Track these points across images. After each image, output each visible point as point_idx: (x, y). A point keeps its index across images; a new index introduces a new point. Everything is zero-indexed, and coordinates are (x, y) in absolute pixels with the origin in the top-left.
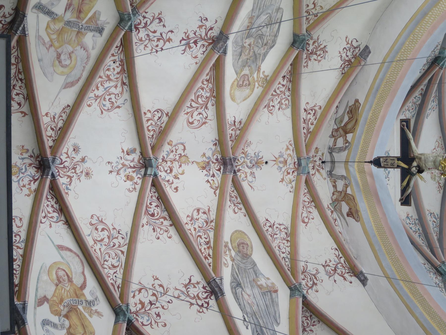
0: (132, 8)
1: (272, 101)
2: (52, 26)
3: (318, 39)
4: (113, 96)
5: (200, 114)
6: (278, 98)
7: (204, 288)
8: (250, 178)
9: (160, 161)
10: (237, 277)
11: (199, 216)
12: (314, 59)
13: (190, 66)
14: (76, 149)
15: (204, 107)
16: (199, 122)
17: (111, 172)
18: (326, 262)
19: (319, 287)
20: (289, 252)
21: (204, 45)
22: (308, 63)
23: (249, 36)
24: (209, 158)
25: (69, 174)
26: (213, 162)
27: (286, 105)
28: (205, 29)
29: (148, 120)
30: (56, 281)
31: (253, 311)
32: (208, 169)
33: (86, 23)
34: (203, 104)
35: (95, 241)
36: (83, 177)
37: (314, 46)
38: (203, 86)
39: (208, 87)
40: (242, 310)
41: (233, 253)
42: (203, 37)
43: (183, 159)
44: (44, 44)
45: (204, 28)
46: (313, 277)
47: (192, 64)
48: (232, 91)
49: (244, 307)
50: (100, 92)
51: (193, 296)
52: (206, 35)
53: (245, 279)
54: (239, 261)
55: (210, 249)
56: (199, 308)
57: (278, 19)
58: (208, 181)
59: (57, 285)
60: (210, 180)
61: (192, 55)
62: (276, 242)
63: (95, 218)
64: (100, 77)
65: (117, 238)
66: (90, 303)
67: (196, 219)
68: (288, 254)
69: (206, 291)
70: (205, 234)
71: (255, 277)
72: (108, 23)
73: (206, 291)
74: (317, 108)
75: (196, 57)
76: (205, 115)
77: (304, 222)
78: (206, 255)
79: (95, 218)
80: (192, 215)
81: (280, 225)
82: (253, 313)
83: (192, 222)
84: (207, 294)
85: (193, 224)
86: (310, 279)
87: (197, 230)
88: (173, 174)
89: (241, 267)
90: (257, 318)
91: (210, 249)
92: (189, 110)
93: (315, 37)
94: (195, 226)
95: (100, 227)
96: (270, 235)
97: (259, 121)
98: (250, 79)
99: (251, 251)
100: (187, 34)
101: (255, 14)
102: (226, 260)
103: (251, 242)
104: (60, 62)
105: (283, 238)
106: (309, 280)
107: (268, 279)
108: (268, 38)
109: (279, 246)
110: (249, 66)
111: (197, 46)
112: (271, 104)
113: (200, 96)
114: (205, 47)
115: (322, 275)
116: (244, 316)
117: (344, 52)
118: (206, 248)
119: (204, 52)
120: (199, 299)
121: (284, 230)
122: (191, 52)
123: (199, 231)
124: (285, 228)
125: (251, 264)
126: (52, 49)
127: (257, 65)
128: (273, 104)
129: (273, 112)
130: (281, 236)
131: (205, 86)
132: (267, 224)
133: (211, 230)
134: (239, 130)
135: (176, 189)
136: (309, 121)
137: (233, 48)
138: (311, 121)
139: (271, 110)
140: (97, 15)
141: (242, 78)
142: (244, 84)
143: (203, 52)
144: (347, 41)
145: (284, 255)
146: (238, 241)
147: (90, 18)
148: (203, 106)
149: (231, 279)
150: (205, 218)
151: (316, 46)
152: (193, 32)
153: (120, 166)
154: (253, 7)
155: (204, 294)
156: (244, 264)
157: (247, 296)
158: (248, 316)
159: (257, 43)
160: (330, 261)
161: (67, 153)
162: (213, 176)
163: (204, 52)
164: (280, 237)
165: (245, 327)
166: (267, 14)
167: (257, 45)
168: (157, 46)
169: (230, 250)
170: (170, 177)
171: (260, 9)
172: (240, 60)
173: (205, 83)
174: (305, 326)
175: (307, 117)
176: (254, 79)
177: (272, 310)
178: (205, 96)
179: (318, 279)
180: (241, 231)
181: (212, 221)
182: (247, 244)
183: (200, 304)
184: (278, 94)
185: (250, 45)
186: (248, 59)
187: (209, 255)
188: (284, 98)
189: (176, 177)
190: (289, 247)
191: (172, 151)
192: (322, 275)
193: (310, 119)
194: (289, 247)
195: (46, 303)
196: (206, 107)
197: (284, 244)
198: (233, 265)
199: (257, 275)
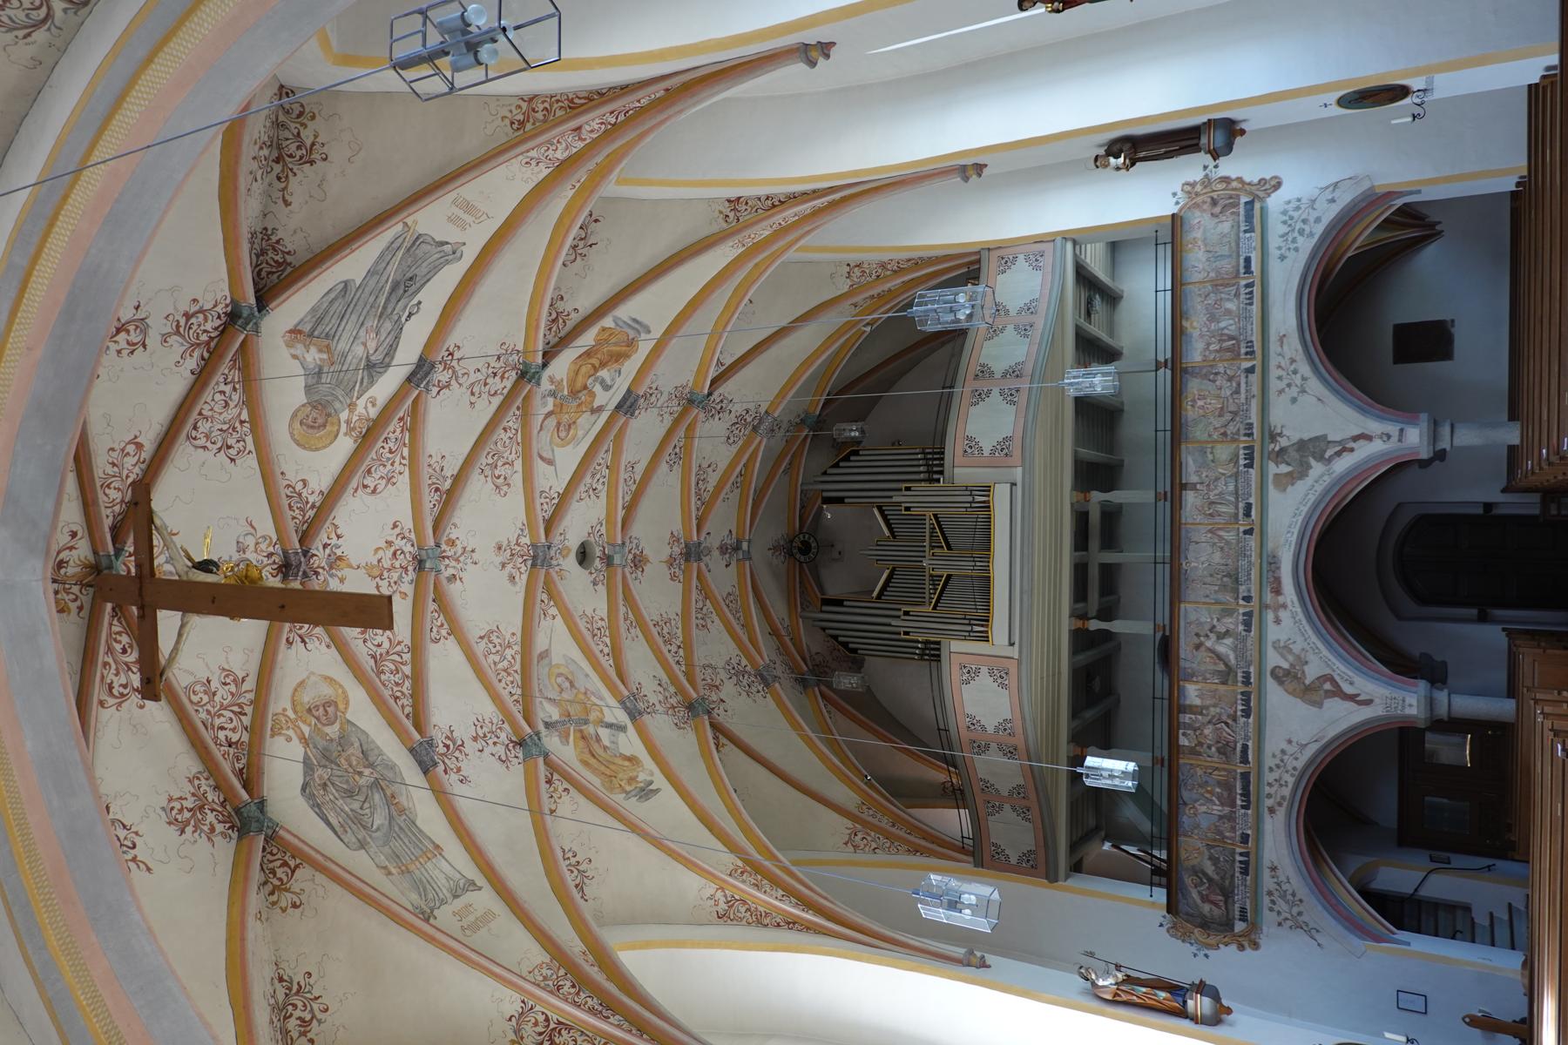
0: (1083, 658)
2: (598, 713)
3: (209, 838)
4: (494, 650)
5: (379, 646)
8: (250, 541)
9: (410, 568)
12: (186, 799)
14: (512, 578)
17: (473, 551)
18: (132, 352)
19: (185, 306)
22: (194, 787)
23: (376, 785)
24: (332, 576)
25: (519, 548)
26: (323, 568)
27: (194, 692)
29: (442, 625)
30: (573, 427)
32: (333, 557)
33: (569, 728)
35: (511, 464)
36: (505, 544)
37: (207, 822)
41: (344, 416)
43: (376, 572)
44: (593, 693)
46: (181, 330)
48: (340, 691)
50: (509, 652)
58: (339, 537)
59: (574, 423)
60: (335, 538)
63: (502, 493)
64: (516, 671)
65: (487, 464)
66: (553, 394)
72: (546, 736)
74: (111, 701)
76: (369, 644)
77: (139, 446)
79: (502, 493)
81: (204, 448)
86: (190, 328)
88: (393, 549)
90: (385, 308)
92: (398, 648)
93: (218, 839)
95: (501, 480)
98: (314, 721)
101: (401, 820)
102: (366, 408)
104: (567, 678)
106: (195, 327)
107: (295, 357)
108: (332, 797)
110: (332, 740)
112: (233, 688)
115: (158, 326)
117: (125, 838)
123: (388, 459)
124: (195, 439)
126: (583, 690)
127: (315, 747)
128: (226, 688)
131: (395, 689)
135: (395, 526)
136: (117, 669)
138: (113, 671)
139: (227, 676)
140: (564, 740)
142: (321, 709)
144: (141, 865)
145: (222, 387)
147: (569, 734)
151: (204, 825)
153: (462, 559)
158: (400, 317)
159: (347, 782)
160: (119, 352)
161: (521, 573)
162: (325, 546)
165: (421, 306)
166: (378, 829)
168: (481, 727)
169: (348, 422)
170: (399, 543)
171: (401, 828)
172: (357, 745)
173: (399, 694)
175: (128, 677)
177: (338, 306)
178: (388, 674)
179: (175, 324)
180: (305, 448)
184: (225, 709)
188: (205, 705)
189: (390, 543)
191: (395, 583)
192: (158, 326)
193: (117, 674)
196: (374, 657)
197: (212, 410)
198: (358, 398)
199: (317, 370)
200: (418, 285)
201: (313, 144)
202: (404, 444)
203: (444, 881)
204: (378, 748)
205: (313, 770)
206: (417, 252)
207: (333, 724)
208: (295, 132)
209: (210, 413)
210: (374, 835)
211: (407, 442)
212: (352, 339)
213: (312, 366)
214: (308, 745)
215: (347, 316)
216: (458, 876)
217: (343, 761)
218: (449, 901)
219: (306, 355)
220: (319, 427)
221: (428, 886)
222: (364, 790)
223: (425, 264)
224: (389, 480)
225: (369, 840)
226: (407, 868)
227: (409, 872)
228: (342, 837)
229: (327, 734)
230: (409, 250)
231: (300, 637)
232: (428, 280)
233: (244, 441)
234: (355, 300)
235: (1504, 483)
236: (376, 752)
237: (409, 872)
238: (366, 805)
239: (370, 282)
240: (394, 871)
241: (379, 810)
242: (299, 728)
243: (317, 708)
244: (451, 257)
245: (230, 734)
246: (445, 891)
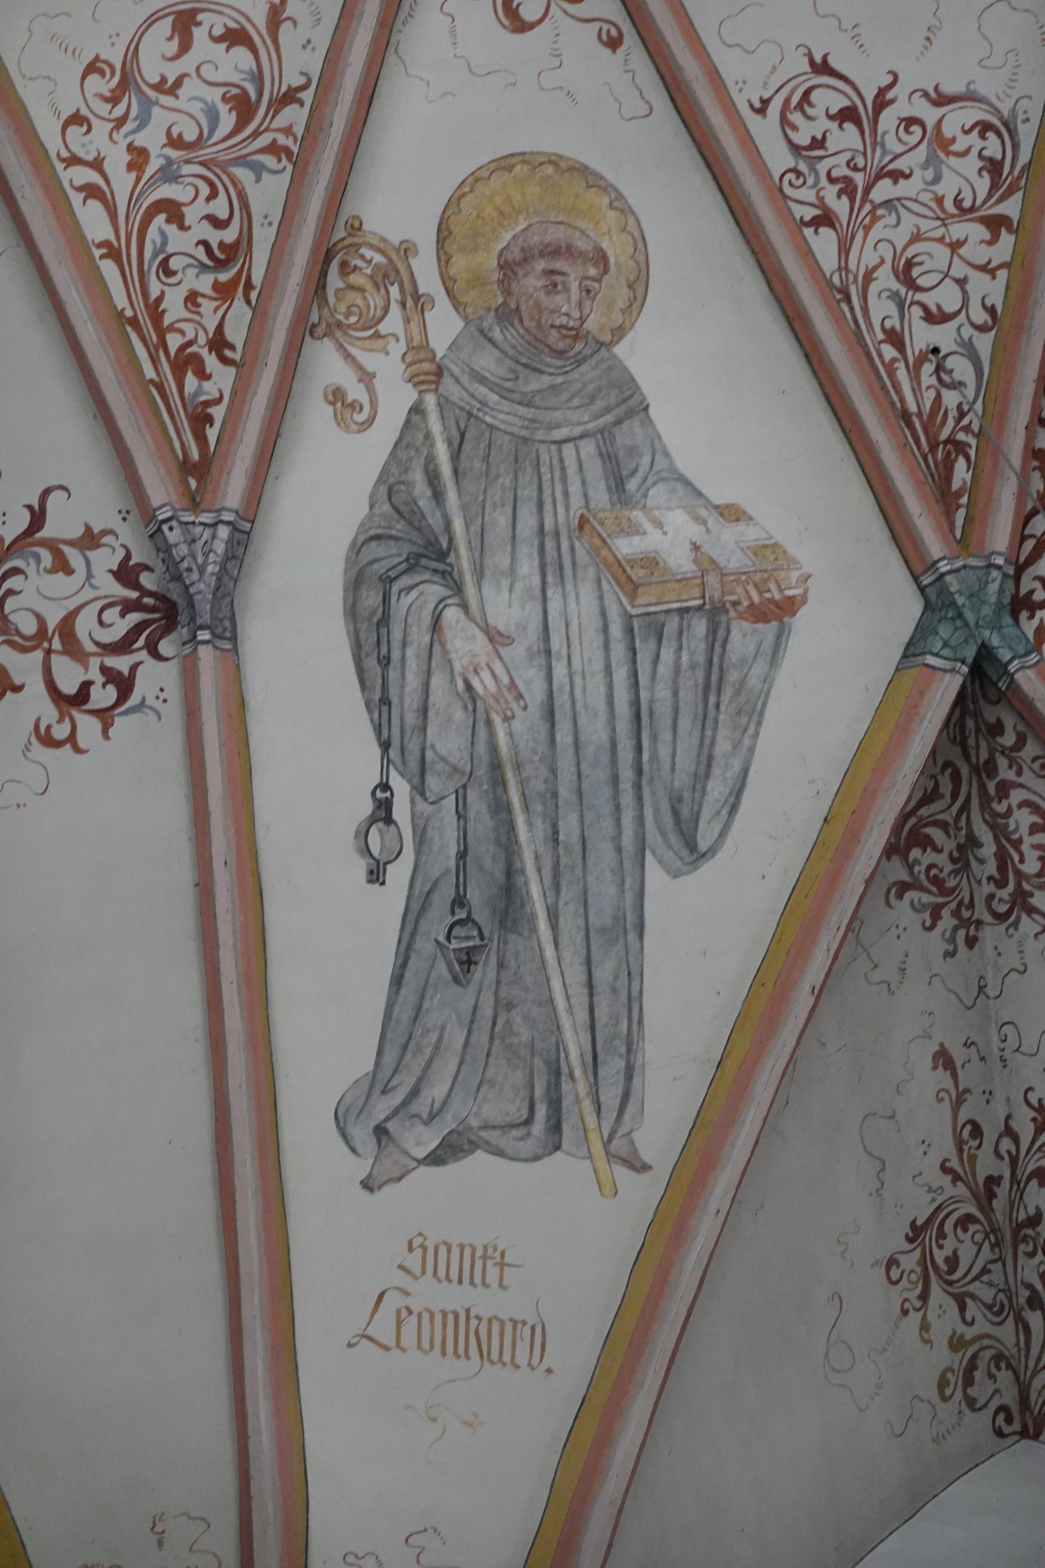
7: (126, 574)
10: (425, 503)
11: (187, 64)
20: (992, 311)
31: (493, 748)
40: (385, 746)
49: (411, 719)
51: (29, 626)
53: (502, 520)
54: (482, 380)
55: (239, 302)
56: (49, 712)
62: (888, 234)
67: (160, 87)
68: (982, 329)
69: (134, 595)
70: (213, 195)
71: (600, 496)
73: (134, 595)
78: (190, 343)
80: (133, 52)
81: (941, 100)
82: (482, 771)
83: (119, 110)
84: (134, 618)
85: (130, 125)
87: (154, 165)
89: (492, 427)
90: (501, 808)
91: (239, 302)
94: (140, 140)
96: (832, 180)
99: (621, 304)
102: (366, 378)
103: (641, 241)
105: (958, 202)
107: (732, 514)
109: (910, 265)
116: (385, 786)
118: (208, 290)
120: (72, 648)
121: (979, 144)
123: (168, 174)
124: (984, 128)
125: (599, 404)
130: (939, 189)
132: (814, 96)
133: (269, 161)
145: (944, 336)
146: (508, 236)
149: (370, 516)
150: (235, 78)
155: (111, 615)
156: (528, 405)
157: (481, 639)
158: (420, 789)
164: (926, 197)
165: (360, 867)
174: (1027, 878)
180: (554, 160)
181: (290, 97)
182: (601, 259)
183: (69, 686)
187: (219, 343)
190: (1002, 275)
194: (1002, 275)
195: (1037, 448)
197: (955, 246)
198: (417, 409)
199: (632, 485)
200: (424, 946)
201: (924, 1296)
202: (113, 253)
206: (519, 1077)
208: (973, 1309)
209: (958, 230)
211: (109, 269)
212: (557, 642)
213: (657, 494)
215: (624, 727)
219: (694, 531)
220: (527, 258)
223: (457, 1037)
224: (127, 83)
230: (555, 1071)
232: (397, 980)
233: (796, 149)
234: (627, 799)
235: (382, 356)
239: (612, 890)
244: (382, 1108)
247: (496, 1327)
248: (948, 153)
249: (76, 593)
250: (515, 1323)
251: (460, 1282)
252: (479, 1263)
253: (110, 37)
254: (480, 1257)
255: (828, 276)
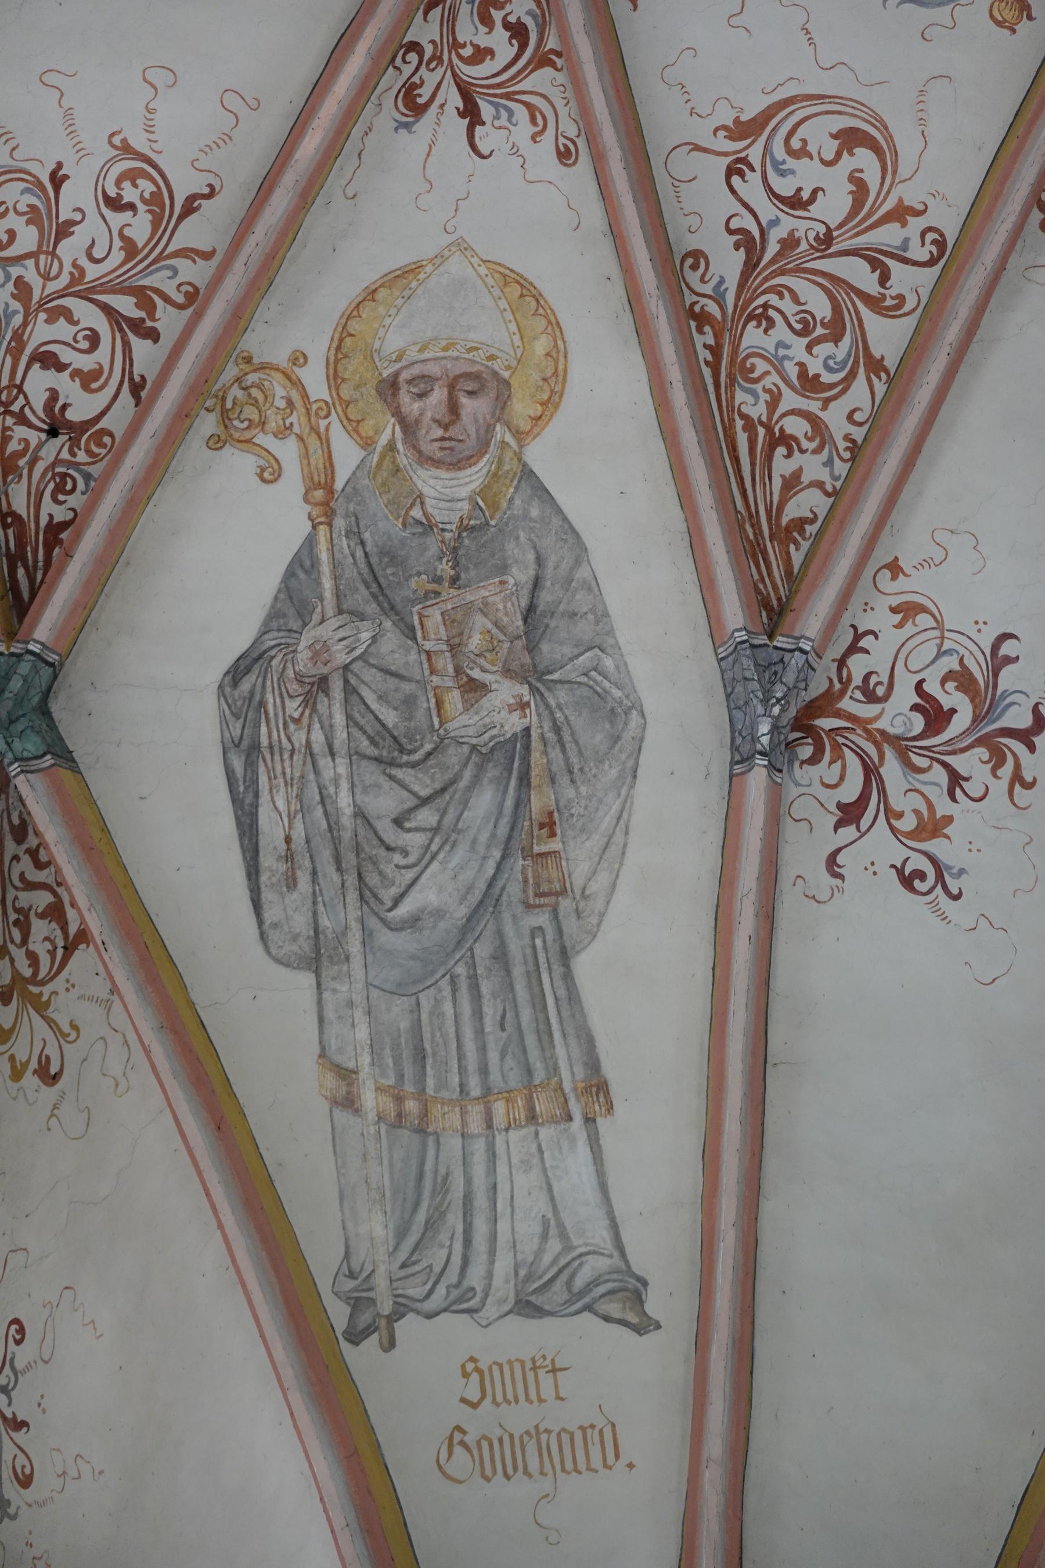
1: (130, 249)
5: (796, 202)
6: (84, 262)
13: (938, 555)
15: (773, 248)
16: (795, 144)
21: (871, 697)
28: (893, 815)
34: (782, 272)
38: (813, 406)
39: (765, 397)
42: (889, 753)
45: (900, 815)
47: (926, 563)
48: (541, 345)
52: (871, 772)
57: (291, 883)
61: (939, 625)
75: (907, 611)
76: (751, 188)
92: (888, 236)
97: (231, 100)
98: (389, 430)
100: (1007, 771)
108: (318, 737)
110: (428, 526)
111: (919, 686)
112: (140, 227)
113: (819, 331)
114: (857, 680)
119: (853, 649)
122: (947, 645)
127: (354, 533)
128: (117, 219)
129: (111, 161)
131: (790, 400)
134: (414, 47)
137: (622, 666)
139: (132, 176)
141: (472, 442)
142: (439, 395)
143: (862, 644)
148: (779, 255)
152: (974, 788)
154: (568, 976)
159: (410, 702)
163: (853, 649)
166: (413, 922)
167: (408, 688)
171: (501, 956)
172: (521, 575)
173: (796, 426)
176: (353, 427)
178: (781, 332)
185: (473, 689)
186: (454, 581)
203: (528, 1230)
204: (602, 615)
205: (304, 613)
207: (457, 465)
210: (385, 937)
214: (330, 514)
216: (601, 1237)
217: (435, 617)
218: (491, 1311)
221: (455, 1220)
222: (453, 756)
225: (355, 947)
226: (425, 1114)
227: (421, 1131)
228: (268, 896)
229: (421, 498)
231: (466, 92)
236: (584, 629)
237: (421, 1131)
238: (426, 817)
240: (369, 1099)
241: (460, 854)
242: (326, 443)
243: (423, 386)
245: (67, 387)
246: (503, 1265)
247: (565, 1438)
248: (43, 983)
249: (908, 640)
250: (583, 1429)
251: (517, 1401)
252: (530, 1376)
253: (970, 850)
254: (531, 1369)
255: (849, 464)
